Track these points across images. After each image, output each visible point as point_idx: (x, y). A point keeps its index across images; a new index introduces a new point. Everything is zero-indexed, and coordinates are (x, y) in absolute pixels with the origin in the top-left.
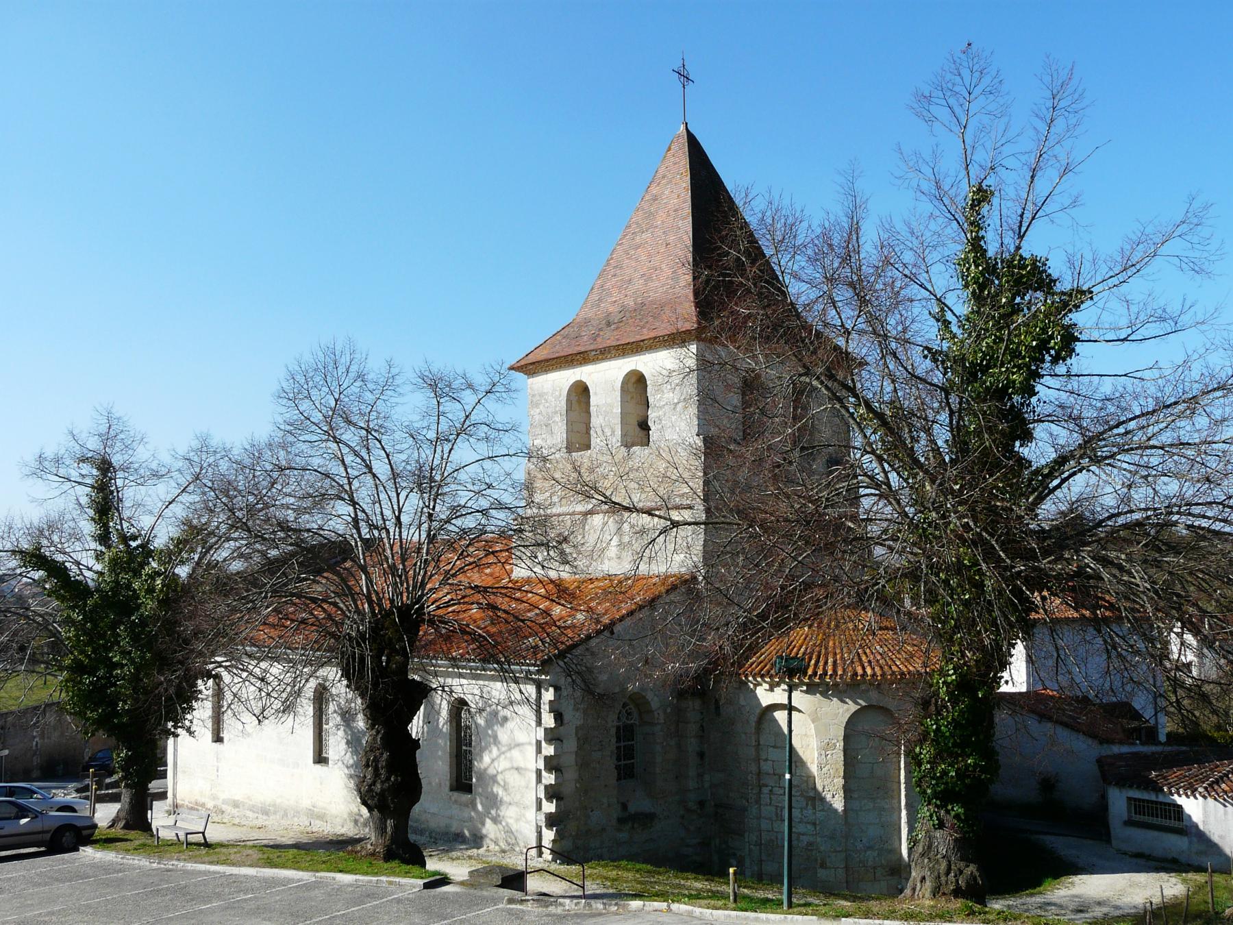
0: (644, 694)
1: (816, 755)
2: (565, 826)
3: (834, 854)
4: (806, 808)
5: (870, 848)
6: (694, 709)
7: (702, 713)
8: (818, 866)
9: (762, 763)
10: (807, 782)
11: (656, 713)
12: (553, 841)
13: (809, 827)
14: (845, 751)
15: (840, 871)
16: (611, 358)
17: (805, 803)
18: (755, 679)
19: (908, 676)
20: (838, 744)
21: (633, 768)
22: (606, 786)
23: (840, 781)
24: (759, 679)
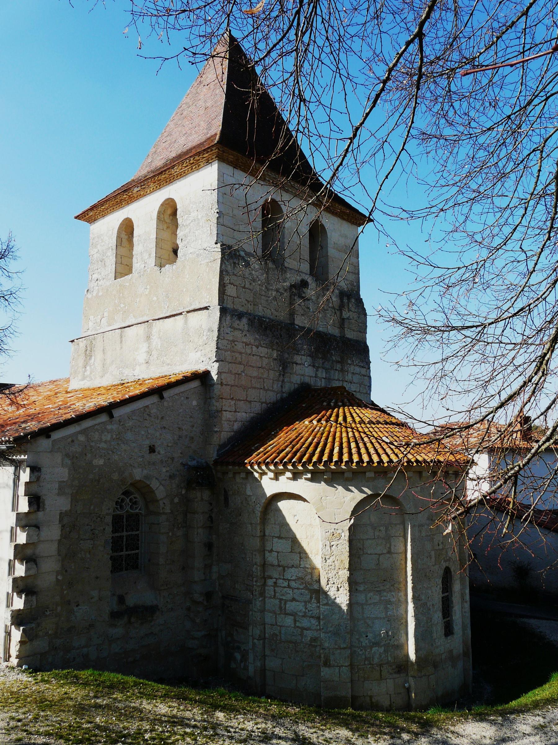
0: (148, 483)
1: (321, 546)
2: (38, 625)
3: (339, 651)
4: (310, 602)
5: (377, 644)
6: (202, 499)
7: (211, 504)
8: (322, 663)
9: (267, 554)
10: (311, 574)
11: (161, 503)
12: (19, 642)
13: (313, 621)
14: (351, 541)
15: (344, 669)
16: (151, 192)
17: (309, 597)
18: (260, 467)
19: (415, 464)
20: (343, 535)
21: (137, 558)
22: (97, 578)
23: (345, 574)
24: (264, 467)
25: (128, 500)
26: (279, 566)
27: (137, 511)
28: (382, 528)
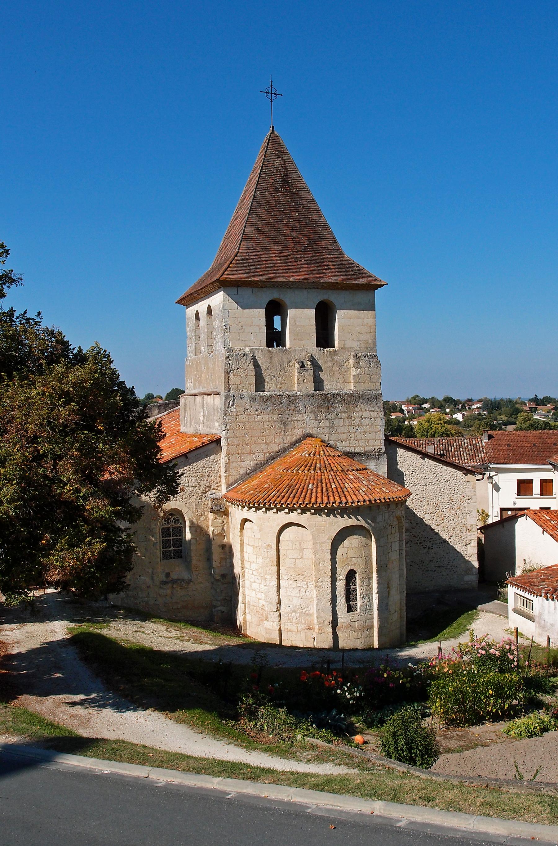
3: (272, 613)
21: (181, 552)
25: (172, 519)
26: (249, 561)
27: (179, 525)
28: (297, 543)
